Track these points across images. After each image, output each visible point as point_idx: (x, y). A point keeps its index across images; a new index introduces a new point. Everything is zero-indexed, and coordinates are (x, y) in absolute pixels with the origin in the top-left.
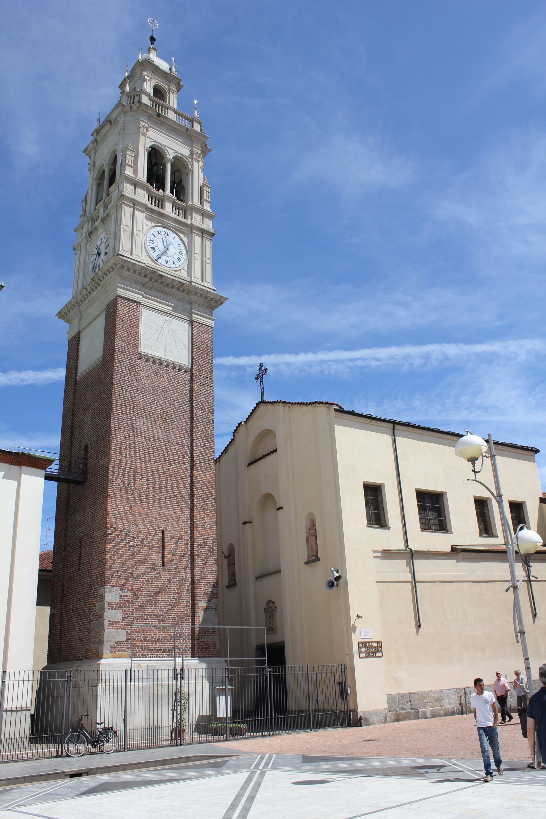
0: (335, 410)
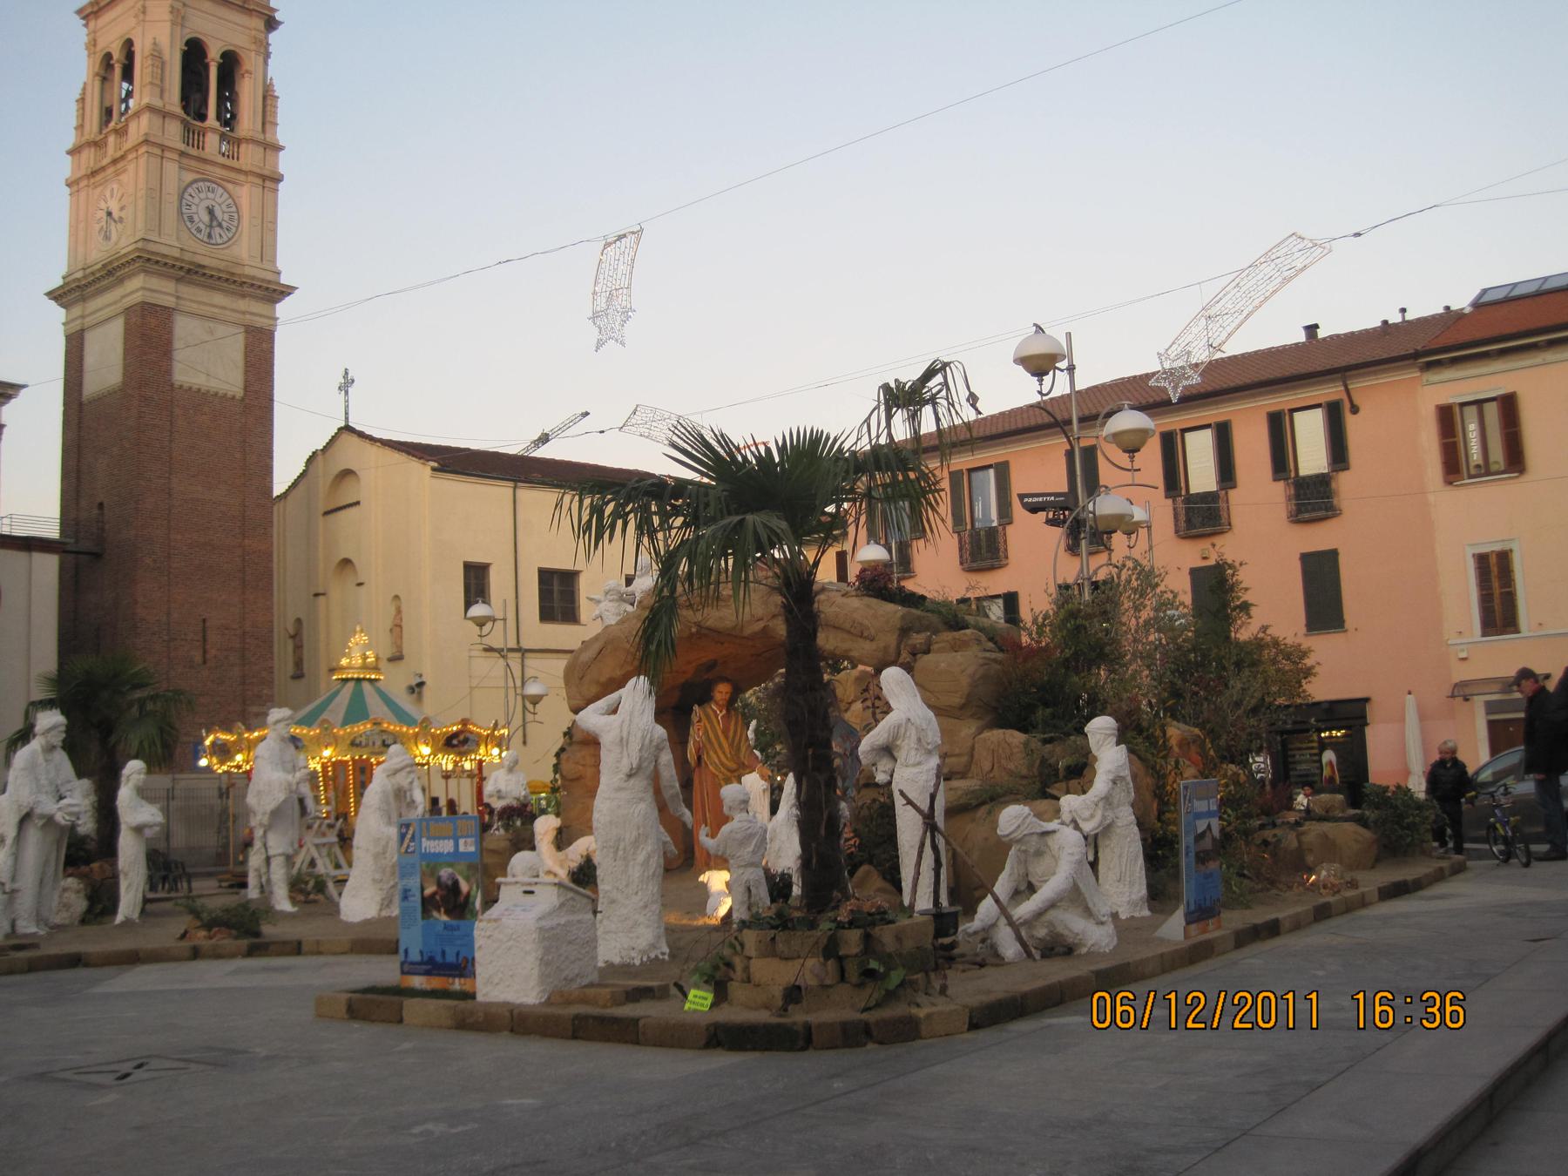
0: (434, 469)
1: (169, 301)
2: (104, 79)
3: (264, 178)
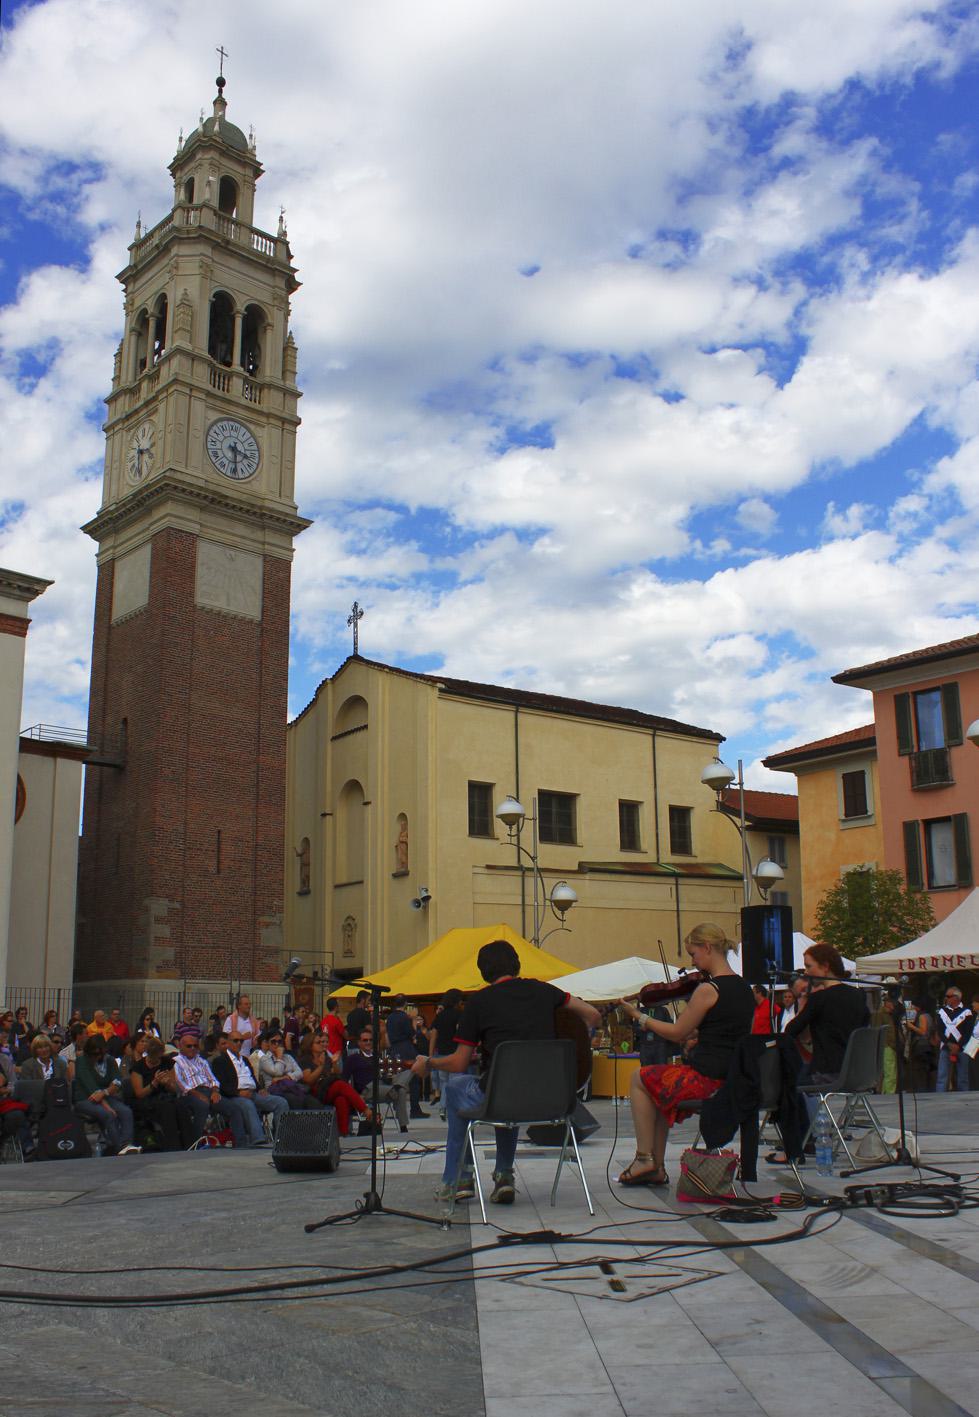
0: (441, 690)
1: (195, 528)
2: (139, 335)
3: (284, 421)
